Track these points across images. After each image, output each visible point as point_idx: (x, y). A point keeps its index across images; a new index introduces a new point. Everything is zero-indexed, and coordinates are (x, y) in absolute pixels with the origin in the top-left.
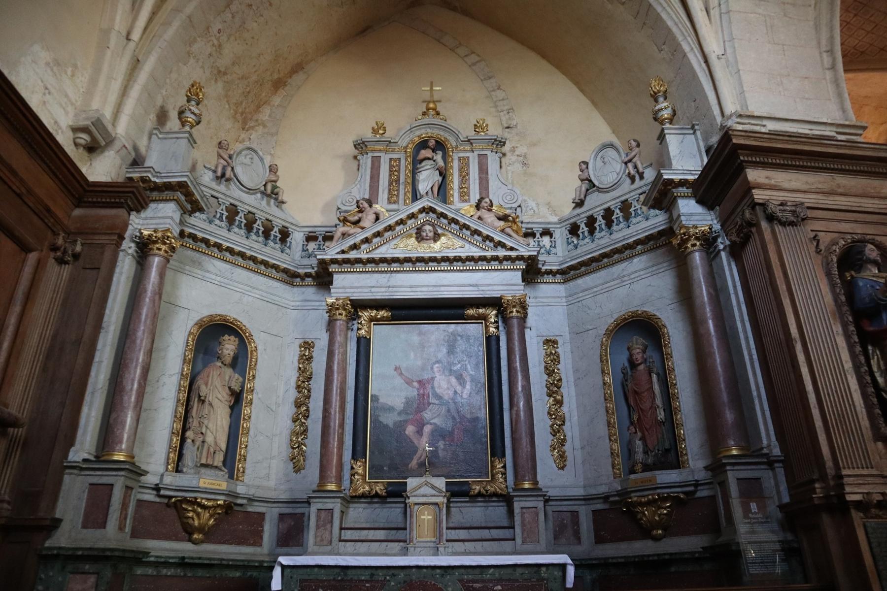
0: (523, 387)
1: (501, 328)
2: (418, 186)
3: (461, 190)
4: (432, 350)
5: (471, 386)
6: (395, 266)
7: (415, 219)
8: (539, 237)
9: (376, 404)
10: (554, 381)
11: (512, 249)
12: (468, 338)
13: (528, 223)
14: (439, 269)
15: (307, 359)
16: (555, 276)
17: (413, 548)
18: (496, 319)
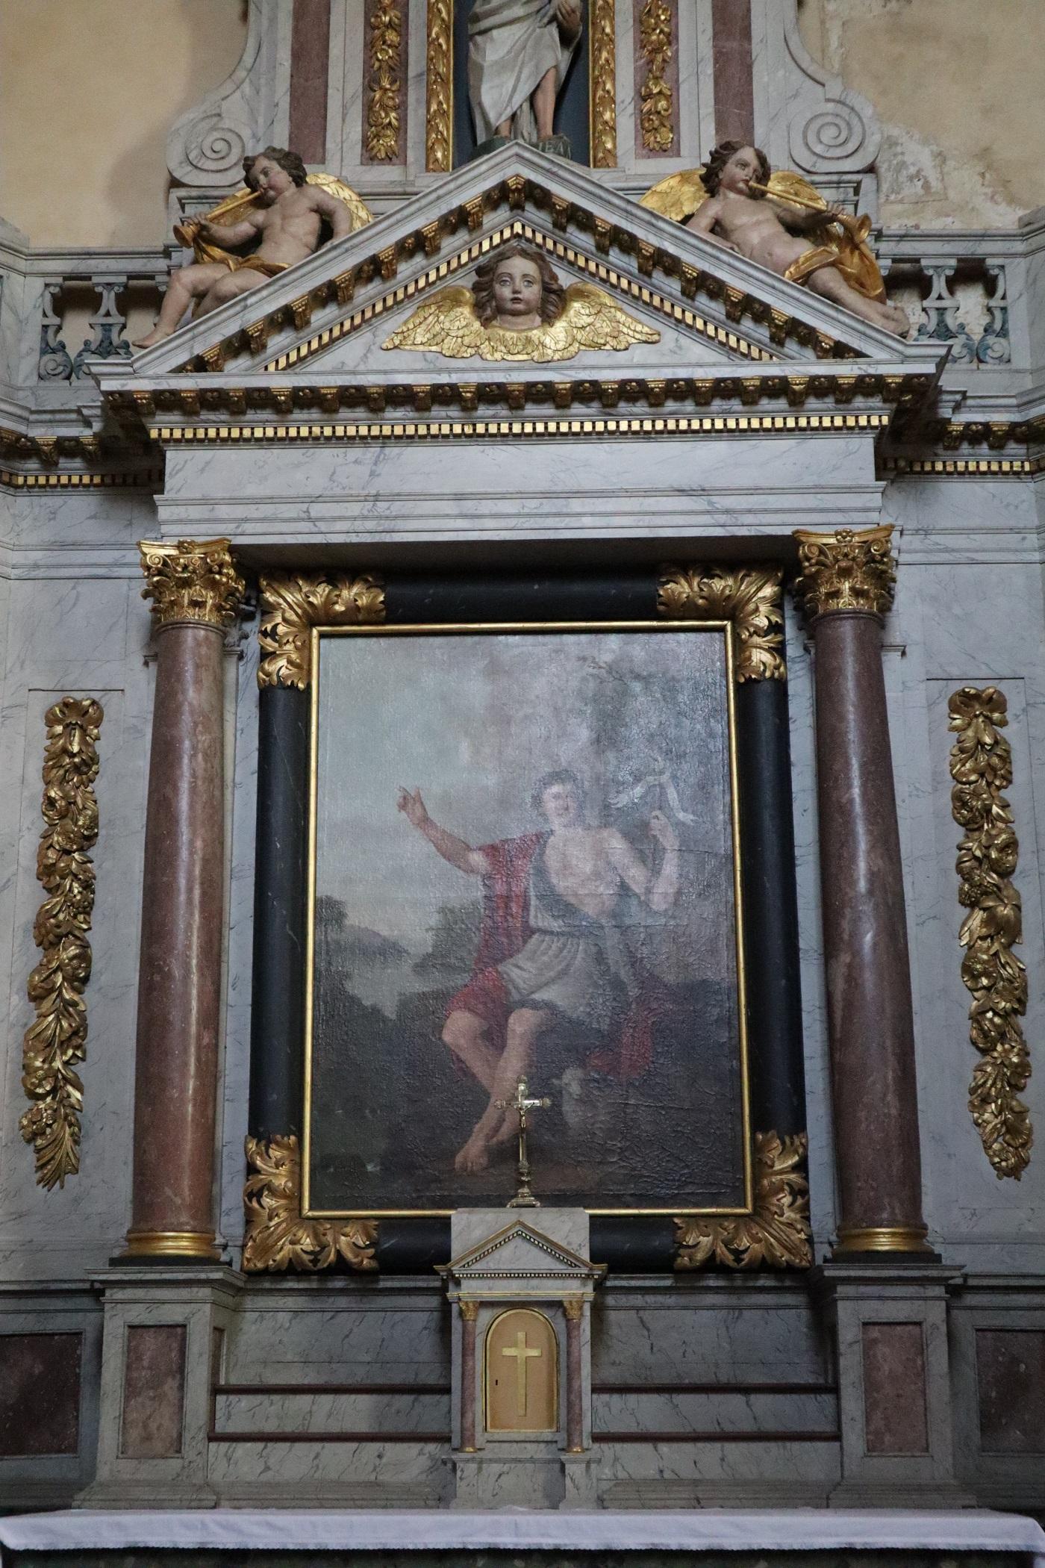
0: (872, 876)
1: (792, 651)
2: (479, 88)
3: (647, 106)
4: (537, 731)
5: (681, 867)
6: (397, 420)
7: (471, 230)
8: (945, 293)
9: (332, 935)
10: (988, 848)
11: (840, 351)
12: (670, 688)
13: (902, 237)
14: (564, 428)
15: (77, 769)
16: (1001, 447)
17: (474, 1466)
18: (774, 619)
